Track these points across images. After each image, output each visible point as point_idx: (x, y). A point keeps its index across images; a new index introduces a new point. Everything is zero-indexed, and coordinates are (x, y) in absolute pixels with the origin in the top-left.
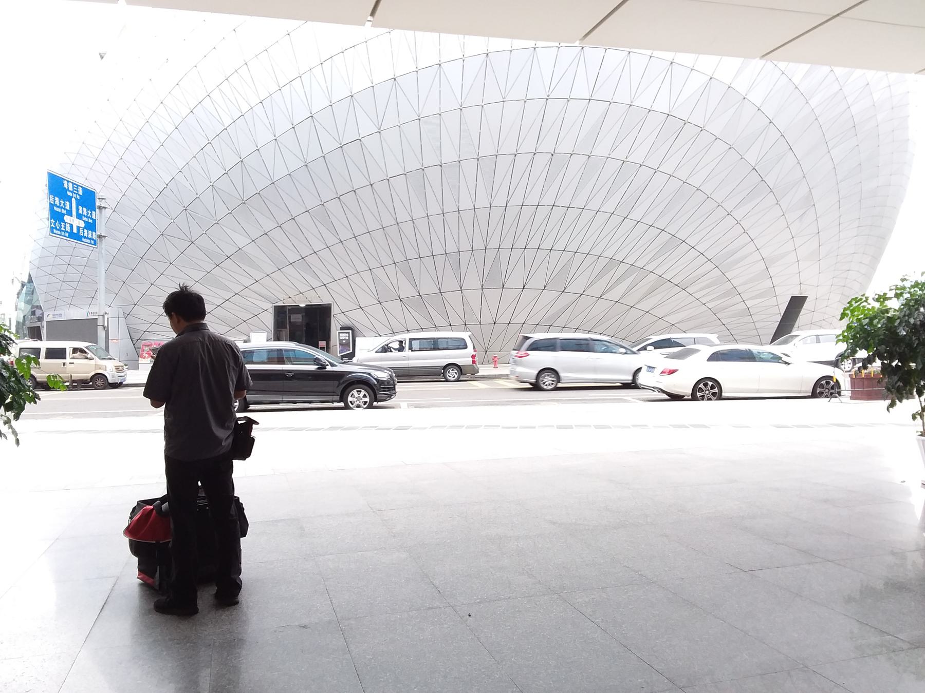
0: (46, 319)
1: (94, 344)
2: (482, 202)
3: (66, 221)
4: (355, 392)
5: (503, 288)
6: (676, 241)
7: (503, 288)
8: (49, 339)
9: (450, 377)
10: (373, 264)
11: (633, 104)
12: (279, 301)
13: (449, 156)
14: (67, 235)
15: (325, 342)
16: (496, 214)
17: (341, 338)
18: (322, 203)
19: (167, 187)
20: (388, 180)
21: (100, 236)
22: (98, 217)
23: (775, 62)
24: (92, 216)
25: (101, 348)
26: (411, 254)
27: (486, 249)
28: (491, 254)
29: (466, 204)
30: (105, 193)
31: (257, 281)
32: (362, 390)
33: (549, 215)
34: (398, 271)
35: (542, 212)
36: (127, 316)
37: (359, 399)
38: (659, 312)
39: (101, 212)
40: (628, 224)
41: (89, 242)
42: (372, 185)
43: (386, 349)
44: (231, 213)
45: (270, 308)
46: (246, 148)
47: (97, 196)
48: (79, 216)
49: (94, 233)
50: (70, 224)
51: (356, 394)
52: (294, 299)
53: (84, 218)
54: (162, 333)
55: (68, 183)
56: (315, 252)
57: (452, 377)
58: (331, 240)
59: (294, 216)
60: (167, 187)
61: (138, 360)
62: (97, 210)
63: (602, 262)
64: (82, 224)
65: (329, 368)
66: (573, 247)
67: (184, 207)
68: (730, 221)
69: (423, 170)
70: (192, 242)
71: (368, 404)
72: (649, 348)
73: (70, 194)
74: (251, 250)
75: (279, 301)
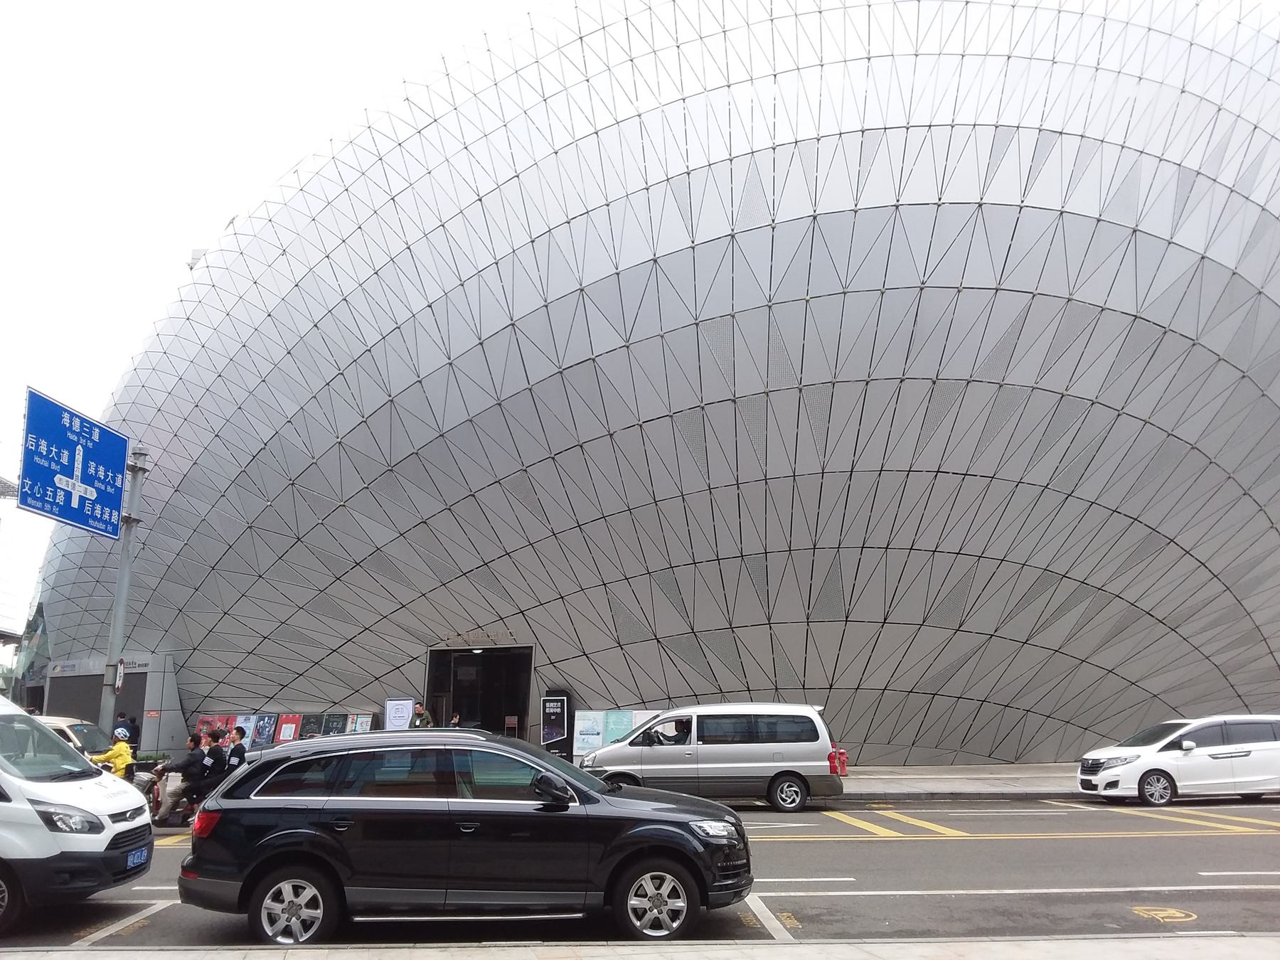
0: (50, 673)
1: (85, 722)
3: (58, 485)
5: (846, 621)
6: (1159, 539)
7: (846, 621)
9: (784, 800)
10: (610, 574)
11: (1074, 297)
12: (439, 641)
13: (749, 384)
14: (56, 509)
15: (517, 717)
16: (834, 487)
17: (547, 711)
18: (524, 468)
20: (641, 426)
21: (128, 521)
22: (127, 486)
23: (227, 758)
24: (114, 481)
25: (102, 732)
27: (814, 549)
28: (824, 559)
31: (404, 606)
32: (668, 876)
35: (918, 484)
36: (179, 669)
38: (1132, 672)
39: (134, 478)
40: (1074, 507)
43: (649, 738)
44: (367, 488)
45: (421, 651)
46: (400, 379)
47: (132, 446)
48: (87, 479)
49: (115, 513)
50: (63, 490)
51: (649, 888)
52: (465, 637)
53: (97, 484)
56: (508, 554)
57: (789, 801)
58: (537, 531)
60: (264, 448)
62: (128, 475)
63: (1030, 576)
64: (92, 494)
65: (575, 807)
66: (974, 548)
67: (291, 480)
68: (1247, 506)
69: (703, 408)
71: (682, 917)
72: (1186, 744)
74: (397, 551)
75: (439, 641)
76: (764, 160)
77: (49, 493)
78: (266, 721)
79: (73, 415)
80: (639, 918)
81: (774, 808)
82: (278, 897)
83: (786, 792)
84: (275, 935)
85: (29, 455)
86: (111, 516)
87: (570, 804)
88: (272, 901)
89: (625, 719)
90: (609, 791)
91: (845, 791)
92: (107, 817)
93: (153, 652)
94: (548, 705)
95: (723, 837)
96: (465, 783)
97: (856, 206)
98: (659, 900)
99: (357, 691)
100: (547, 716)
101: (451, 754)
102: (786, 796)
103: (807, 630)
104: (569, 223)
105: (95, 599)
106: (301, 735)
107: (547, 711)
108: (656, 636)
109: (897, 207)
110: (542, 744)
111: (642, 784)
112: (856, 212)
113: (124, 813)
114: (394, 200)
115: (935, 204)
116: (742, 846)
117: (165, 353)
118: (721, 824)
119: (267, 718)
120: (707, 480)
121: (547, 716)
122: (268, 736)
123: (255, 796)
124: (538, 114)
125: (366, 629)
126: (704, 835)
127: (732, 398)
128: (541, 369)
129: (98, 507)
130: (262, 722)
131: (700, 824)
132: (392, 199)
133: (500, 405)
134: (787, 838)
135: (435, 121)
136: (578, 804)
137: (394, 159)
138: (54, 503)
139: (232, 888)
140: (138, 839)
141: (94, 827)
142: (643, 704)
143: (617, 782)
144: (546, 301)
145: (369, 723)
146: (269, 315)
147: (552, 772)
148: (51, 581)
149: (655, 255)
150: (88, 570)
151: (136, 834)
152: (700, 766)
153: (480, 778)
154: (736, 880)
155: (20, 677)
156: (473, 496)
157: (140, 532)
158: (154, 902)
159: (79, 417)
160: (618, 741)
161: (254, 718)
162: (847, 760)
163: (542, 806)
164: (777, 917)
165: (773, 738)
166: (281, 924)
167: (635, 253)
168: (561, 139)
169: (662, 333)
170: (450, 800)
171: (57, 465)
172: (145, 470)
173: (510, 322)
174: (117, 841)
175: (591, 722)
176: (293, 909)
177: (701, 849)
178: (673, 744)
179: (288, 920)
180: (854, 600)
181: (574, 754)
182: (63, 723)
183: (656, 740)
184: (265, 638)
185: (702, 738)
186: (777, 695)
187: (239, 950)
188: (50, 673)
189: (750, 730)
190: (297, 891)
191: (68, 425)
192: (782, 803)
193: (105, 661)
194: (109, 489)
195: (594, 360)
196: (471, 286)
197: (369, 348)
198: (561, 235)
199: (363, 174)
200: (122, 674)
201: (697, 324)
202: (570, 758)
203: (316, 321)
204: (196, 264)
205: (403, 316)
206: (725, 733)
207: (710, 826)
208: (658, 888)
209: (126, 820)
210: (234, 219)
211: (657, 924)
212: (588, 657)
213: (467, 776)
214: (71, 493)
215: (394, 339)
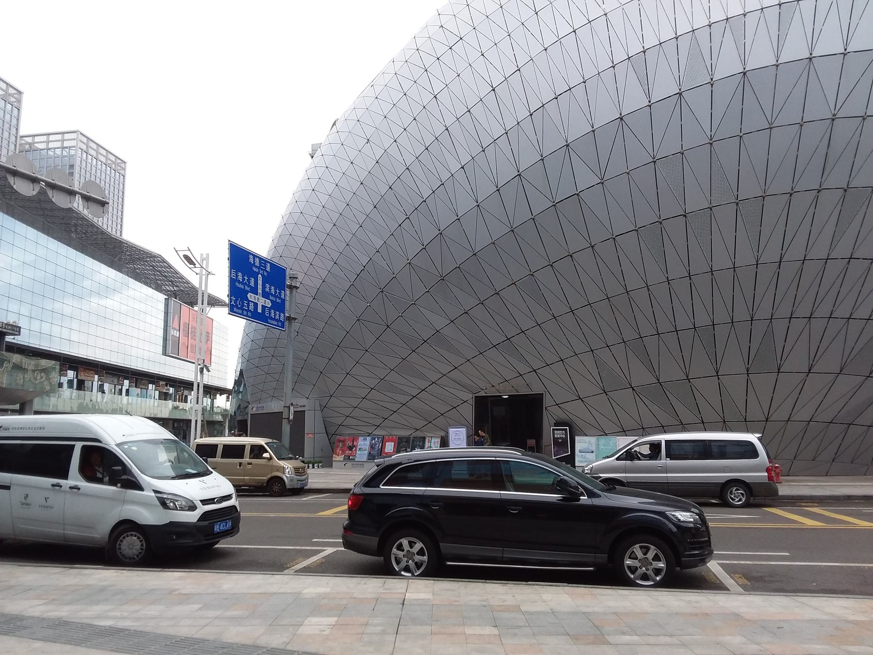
1: (274, 441)
2: (746, 257)
3: (250, 299)
4: (637, 550)
5: (779, 372)
7: (779, 372)
9: (733, 500)
13: (696, 201)
14: (249, 314)
15: (535, 441)
17: (556, 436)
18: (532, 273)
19: (364, 269)
20: (614, 239)
21: (289, 319)
22: (287, 298)
25: (284, 446)
26: (647, 330)
28: (759, 328)
29: (722, 261)
30: (292, 267)
33: (844, 271)
34: (629, 352)
36: (323, 408)
37: (645, 562)
39: (291, 293)
41: (276, 323)
42: (593, 247)
43: (630, 455)
45: (469, 397)
47: (288, 272)
48: (265, 295)
49: (282, 315)
50: (253, 302)
51: (639, 554)
52: (498, 388)
53: (271, 298)
54: (355, 427)
55: (254, 259)
56: (523, 332)
57: (737, 500)
59: (498, 291)
60: (364, 269)
61: (332, 457)
62: (288, 292)
64: (269, 304)
70: (388, 327)
71: (663, 574)
73: (255, 269)
76: (702, 36)
77: (245, 304)
79: (255, 256)
80: (633, 573)
81: (725, 504)
82: (400, 548)
83: (735, 494)
84: (400, 571)
85: (233, 282)
86: (280, 316)
87: (581, 498)
88: (397, 550)
89: (611, 442)
90: (607, 490)
91: (780, 493)
92: (199, 501)
93: (308, 398)
95: (690, 522)
96: (509, 482)
97: (777, 61)
98: (646, 561)
99: (430, 422)
100: (556, 440)
101: (500, 463)
102: (735, 497)
103: (748, 379)
104: (557, 98)
105: (272, 367)
106: (398, 450)
107: (556, 436)
108: (631, 386)
109: (810, 59)
110: (553, 458)
111: (626, 485)
112: (777, 66)
113: (214, 499)
114: (436, 98)
115: (841, 54)
116: (704, 528)
117: (301, 213)
118: (688, 514)
119: (376, 439)
120: (666, 274)
121: (556, 440)
122: (378, 450)
123: (383, 486)
124: (532, 24)
125: (433, 383)
126: (676, 520)
127: (684, 213)
128: (540, 204)
129: (272, 311)
130: (374, 441)
131: (673, 513)
132: (435, 97)
133: (513, 231)
134: (736, 525)
135: (461, 39)
136: (586, 498)
137: (435, 69)
138: (248, 310)
139: (373, 541)
140: (211, 518)
141: (193, 508)
142: (624, 432)
143: (612, 485)
144: (542, 156)
145: (439, 443)
146: (362, 184)
147: (567, 476)
148: (246, 356)
149: (621, 114)
150: (267, 349)
151: (222, 512)
152: (669, 475)
153: (518, 479)
154: (701, 551)
155: (233, 414)
156: (498, 294)
157: (296, 325)
158: (325, 548)
159: (259, 258)
160: (608, 457)
161: (369, 438)
162: (780, 472)
163: (562, 498)
164: (732, 577)
165: (723, 455)
166: (403, 564)
167: (605, 114)
168: (549, 39)
169: (628, 171)
170: (501, 492)
171: (248, 287)
172: (297, 288)
173: (517, 173)
174: (205, 516)
175: (587, 444)
176: (410, 555)
177: (674, 529)
178: (648, 460)
179: (407, 562)
181: (576, 465)
182: (261, 441)
183: (636, 456)
184: (372, 389)
185: (669, 455)
186: (725, 427)
187: (381, 578)
188: (251, 412)
189: (705, 450)
190: (411, 544)
191: (252, 263)
192: (732, 501)
193: (283, 404)
194: (278, 300)
195: (578, 194)
196: (490, 151)
197: (424, 200)
198: (551, 108)
199: (415, 82)
200: (293, 412)
201: (655, 162)
202: (574, 466)
203: (390, 185)
204: (315, 154)
205: (445, 176)
206: (686, 452)
207: (681, 515)
208: (645, 554)
209: (214, 503)
210: (335, 122)
211: (645, 577)
212: (582, 400)
213: (510, 477)
214: (257, 303)
215: (440, 192)
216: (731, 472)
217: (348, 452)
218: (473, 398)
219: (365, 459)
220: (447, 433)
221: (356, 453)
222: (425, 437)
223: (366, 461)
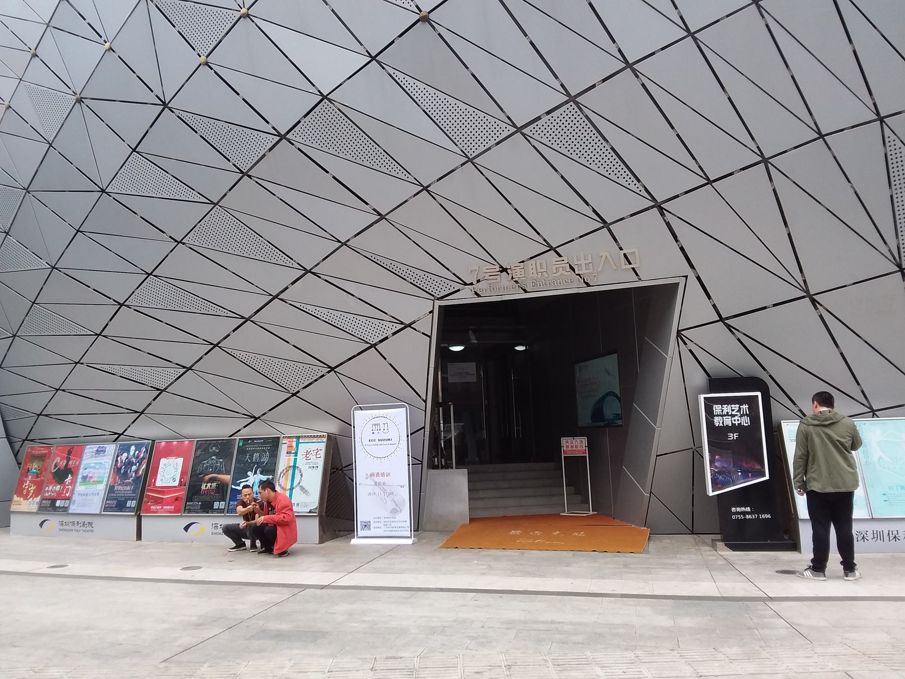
8: (564, 457)
17: (717, 421)
75: (458, 287)
78: (132, 453)
94: (717, 409)
99: (294, 395)
107: (717, 421)
119: (133, 448)
122: (137, 478)
130: (125, 455)
161: (111, 448)
180: (232, 212)
184: (121, 305)
216: (791, 497)
217: (53, 489)
218: (431, 312)
219: (95, 505)
220: (348, 423)
221: (73, 490)
222: (279, 438)
223: (100, 515)
